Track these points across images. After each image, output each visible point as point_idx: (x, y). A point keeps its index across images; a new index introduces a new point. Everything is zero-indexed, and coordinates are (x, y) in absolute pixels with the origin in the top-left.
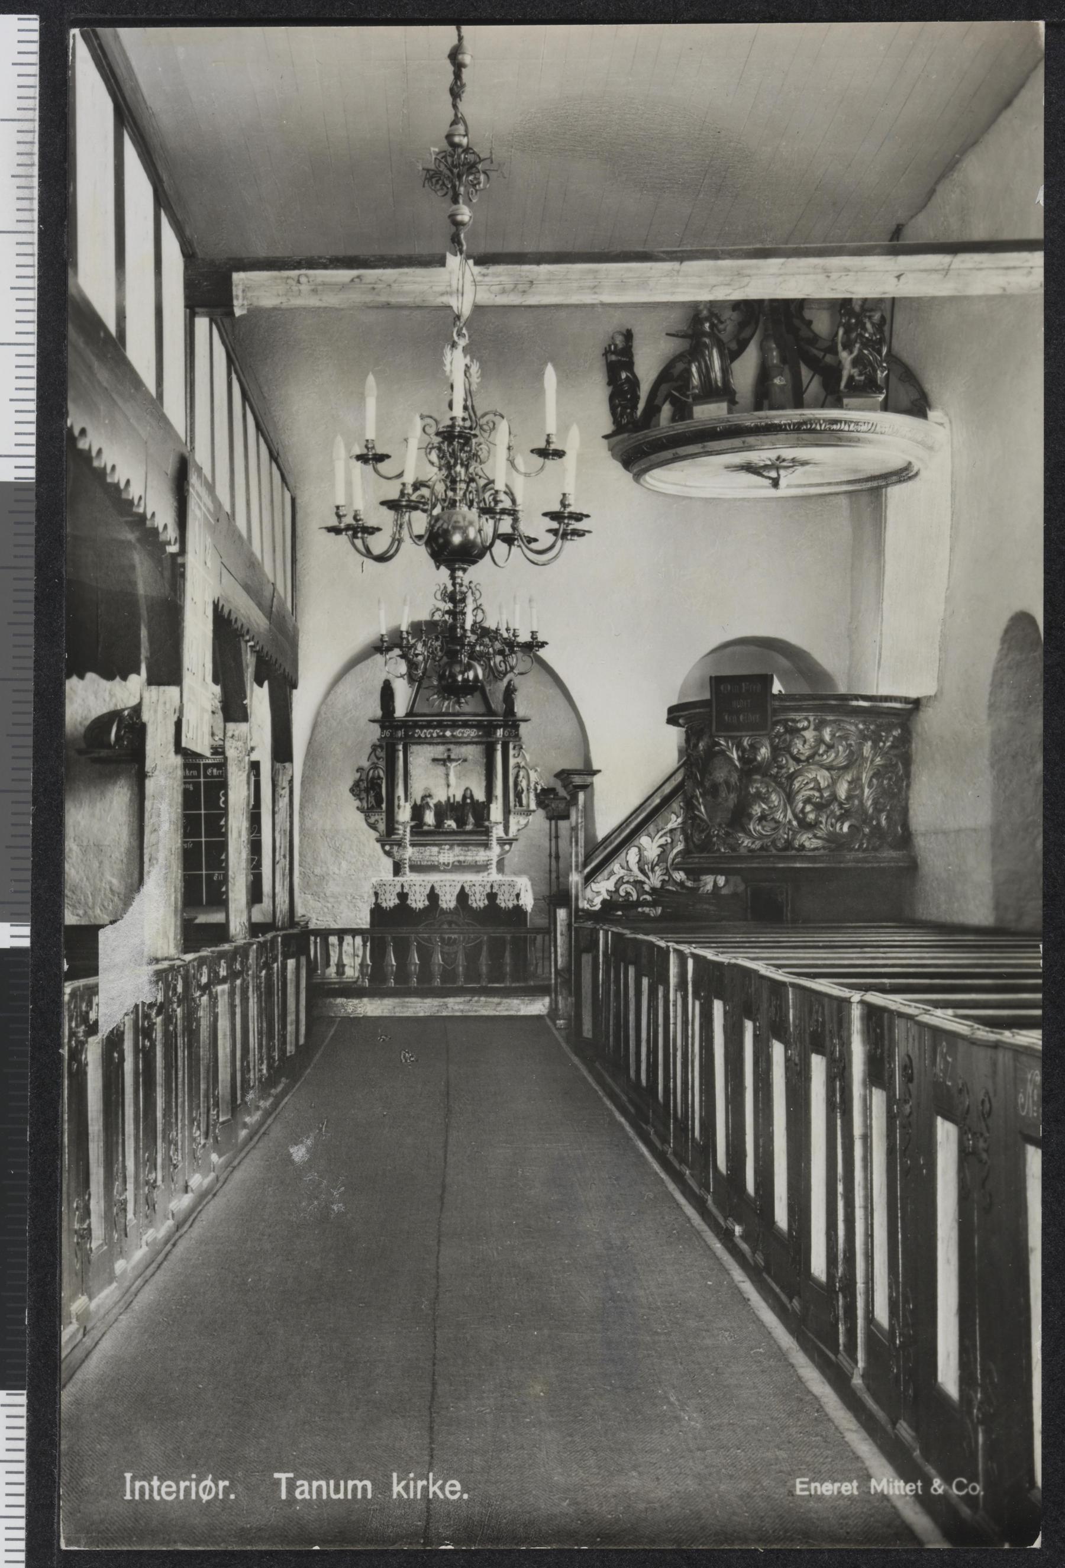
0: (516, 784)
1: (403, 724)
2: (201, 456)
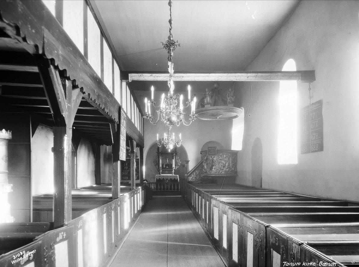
0: (177, 162)
1: (161, 153)
2: (124, 107)
